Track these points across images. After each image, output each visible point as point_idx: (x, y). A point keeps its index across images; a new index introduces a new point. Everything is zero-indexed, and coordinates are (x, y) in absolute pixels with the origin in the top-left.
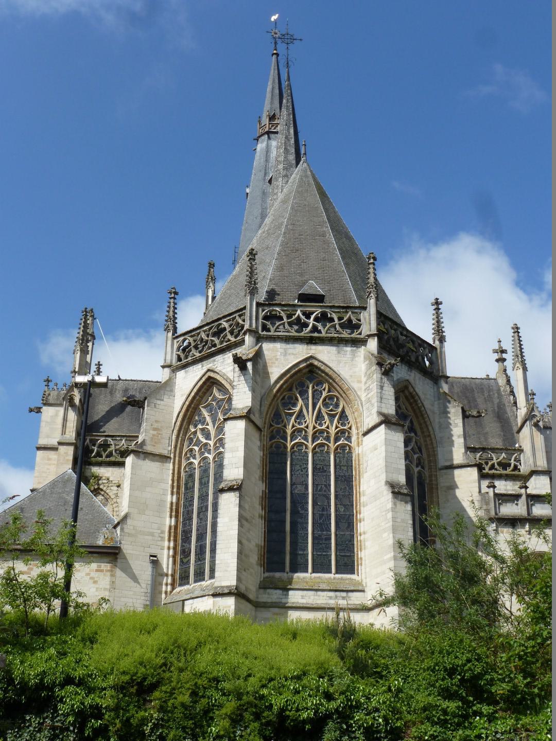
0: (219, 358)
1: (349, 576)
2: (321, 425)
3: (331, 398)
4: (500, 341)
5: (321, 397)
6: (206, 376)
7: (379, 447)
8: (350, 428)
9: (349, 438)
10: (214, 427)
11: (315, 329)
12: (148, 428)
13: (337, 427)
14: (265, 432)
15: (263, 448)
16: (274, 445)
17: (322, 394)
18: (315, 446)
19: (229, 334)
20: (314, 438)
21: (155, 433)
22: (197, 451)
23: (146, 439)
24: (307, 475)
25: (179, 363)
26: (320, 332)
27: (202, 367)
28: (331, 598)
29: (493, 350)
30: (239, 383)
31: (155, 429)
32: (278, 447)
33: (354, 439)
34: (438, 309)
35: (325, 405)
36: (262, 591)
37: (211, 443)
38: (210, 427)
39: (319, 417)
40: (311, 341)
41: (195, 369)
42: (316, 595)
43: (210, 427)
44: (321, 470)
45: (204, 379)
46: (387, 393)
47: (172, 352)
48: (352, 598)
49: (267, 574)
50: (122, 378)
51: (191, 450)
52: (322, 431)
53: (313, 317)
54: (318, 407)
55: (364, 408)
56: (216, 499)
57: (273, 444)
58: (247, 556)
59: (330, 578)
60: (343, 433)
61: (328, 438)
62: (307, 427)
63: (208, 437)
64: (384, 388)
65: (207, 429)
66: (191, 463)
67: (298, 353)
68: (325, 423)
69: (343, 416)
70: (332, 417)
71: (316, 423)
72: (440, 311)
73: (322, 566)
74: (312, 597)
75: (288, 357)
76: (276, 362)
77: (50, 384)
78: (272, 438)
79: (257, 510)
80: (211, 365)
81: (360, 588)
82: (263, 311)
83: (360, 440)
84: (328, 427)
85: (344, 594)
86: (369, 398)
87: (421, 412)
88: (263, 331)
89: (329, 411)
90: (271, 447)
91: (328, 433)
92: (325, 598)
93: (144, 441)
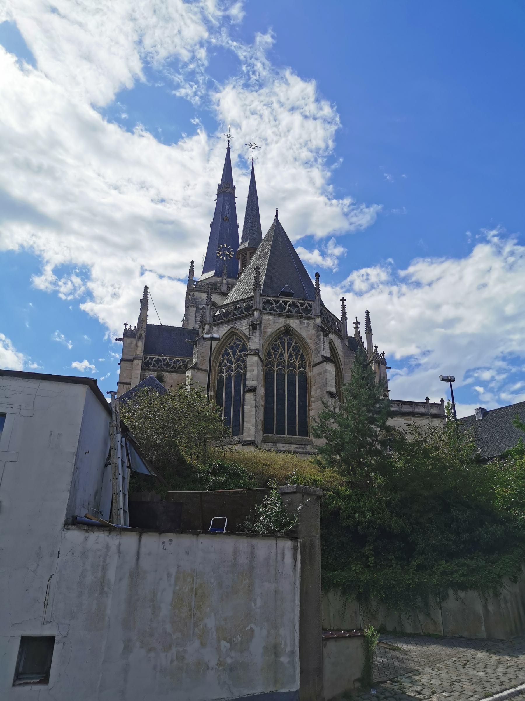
0: (238, 322)
1: (305, 437)
2: (291, 360)
3: (296, 347)
4: (356, 318)
5: (291, 346)
6: (230, 331)
7: (322, 373)
8: (305, 362)
9: (305, 368)
10: (234, 358)
11: (289, 311)
12: (199, 356)
13: (299, 362)
14: (264, 362)
15: (263, 370)
16: (268, 369)
17: (292, 344)
18: (288, 371)
19: (243, 310)
20: (288, 367)
21: (202, 358)
22: (242, 372)
23: (198, 361)
24: (284, 385)
25: (214, 323)
26: (291, 312)
27: (228, 326)
28: (297, 448)
29: (353, 322)
30: (253, 336)
31: (202, 357)
32: (270, 370)
33: (307, 368)
34: (343, 303)
35: (294, 350)
36: (263, 443)
37: (233, 366)
38: (232, 358)
39: (290, 356)
40: (287, 317)
41: (223, 326)
42: (290, 447)
43: (232, 358)
44: (291, 383)
45: (229, 332)
46: (326, 346)
47: (210, 317)
48: (307, 449)
49: (265, 435)
50: (162, 324)
51: (221, 369)
52: (292, 363)
53: (288, 304)
54: (290, 350)
55: (314, 353)
56: (244, 395)
57: (267, 368)
58: (258, 426)
59: (296, 438)
60: (302, 365)
61: (295, 368)
62: (284, 361)
63: (231, 362)
64: (325, 344)
65: (230, 358)
66: (222, 376)
67: (282, 321)
68: (293, 359)
69: (302, 357)
70: (297, 357)
71: (289, 359)
72: (345, 304)
73: (292, 432)
74: (288, 448)
75: (276, 324)
76: (270, 326)
77: (127, 326)
78: (267, 365)
79: (261, 403)
80: (233, 325)
81: (311, 443)
82: (263, 299)
83: (311, 369)
84: (294, 361)
85: (303, 446)
86: (317, 348)
87: (336, 355)
88: (263, 310)
89: (274, 351)
90: (266, 370)
91: (273, 362)
92: (294, 448)
93: (197, 363)
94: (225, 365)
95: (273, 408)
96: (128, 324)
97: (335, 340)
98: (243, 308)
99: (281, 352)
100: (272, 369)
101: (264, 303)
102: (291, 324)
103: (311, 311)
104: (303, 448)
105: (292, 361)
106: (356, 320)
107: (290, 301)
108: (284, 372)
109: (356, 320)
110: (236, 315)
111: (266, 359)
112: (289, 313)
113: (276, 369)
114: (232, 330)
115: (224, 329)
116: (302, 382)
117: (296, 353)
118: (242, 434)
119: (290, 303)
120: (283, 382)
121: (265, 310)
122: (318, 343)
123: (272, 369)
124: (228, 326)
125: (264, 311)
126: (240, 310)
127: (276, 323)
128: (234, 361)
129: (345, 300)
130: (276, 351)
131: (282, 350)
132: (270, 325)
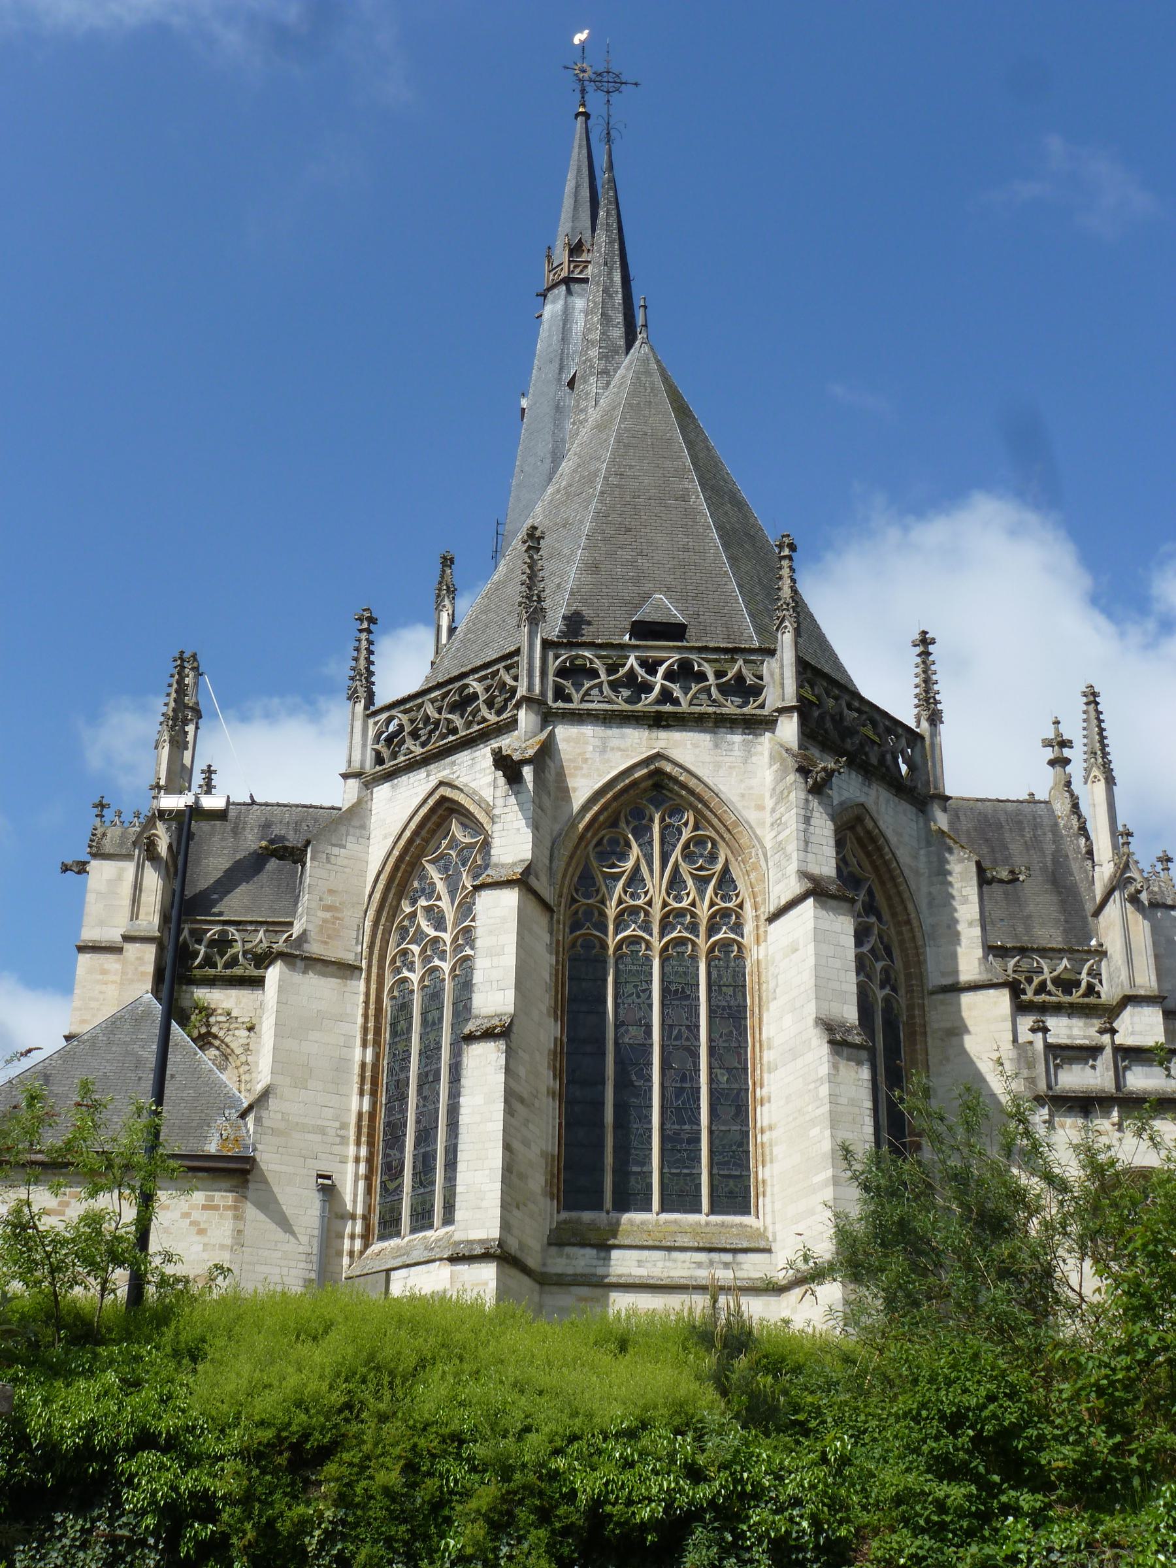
2: (678, 899)
3: (700, 841)
5: (678, 840)
6: (436, 796)
8: (741, 906)
9: (738, 928)
10: (453, 904)
11: (666, 696)
12: (314, 905)
14: (561, 914)
17: (680, 834)
20: (665, 927)
21: (328, 915)
22: (417, 954)
25: (378, 768)
26: (676, 702)
27: (428, 776)
28: (699, 1265)
29: (1044, 741)
30: (506, 810)
33: (748, 928)
34: (926, 654)
37: (447, 937)
39: (675, 882)
40: (658, 721)
45: (431, 802)
47: (364, 746)
49: (565, 1215)
52: (681, 913)
53: (661, 670)
54: (672, 861)
57: (577, 938)
58: (522, 1177)
59: (698, 1224)
60: (724, 917)
61: (693, 928)
63: (440, 924)
65: (438, 907)
68: (688, 894)
69: (726, 881)
72: (931, 658)
74: (660, 1264)
78: (575, 926)
81: (762, 1245)
84: (693, 904)
85: (727, 1257)
86: (780, 843)
87: (890, 871)
90: (573, 945)
92: (687, 1265)
94: (419, 936)
95: (602, 1104)
96: (109, 806)
97: (883, 809)
98: (481, 699)
99: (637, 868)
100: (596, 942)
101: (562, 672)
102: (677, 754)
103: (757, 691)
104: (726, 1265)
105: (684, 904)
106: (1057, 729)
107: (670, 658)
108: (649, 946)
109: (1057, 729)
110: (454, 731)
111: (574, 901)
112: (668, 708)
113: (703, 944)
114: (443, 791)
115: (415, 791)
116: (724, 989)
117: (701, 868)
118: (448, 1220)
119: (672, 665)
120: (644, 991)
121: (564, 701)
122: (784, 819)
123: (596, 942)
124: (428, 776)
125: (560, 704)
126: (469, 709)
127: (612, 749)
128: (450, 915)
129: (933, 641)
130: (701, 868)
131: (477, 842)
132: (585, 760)
